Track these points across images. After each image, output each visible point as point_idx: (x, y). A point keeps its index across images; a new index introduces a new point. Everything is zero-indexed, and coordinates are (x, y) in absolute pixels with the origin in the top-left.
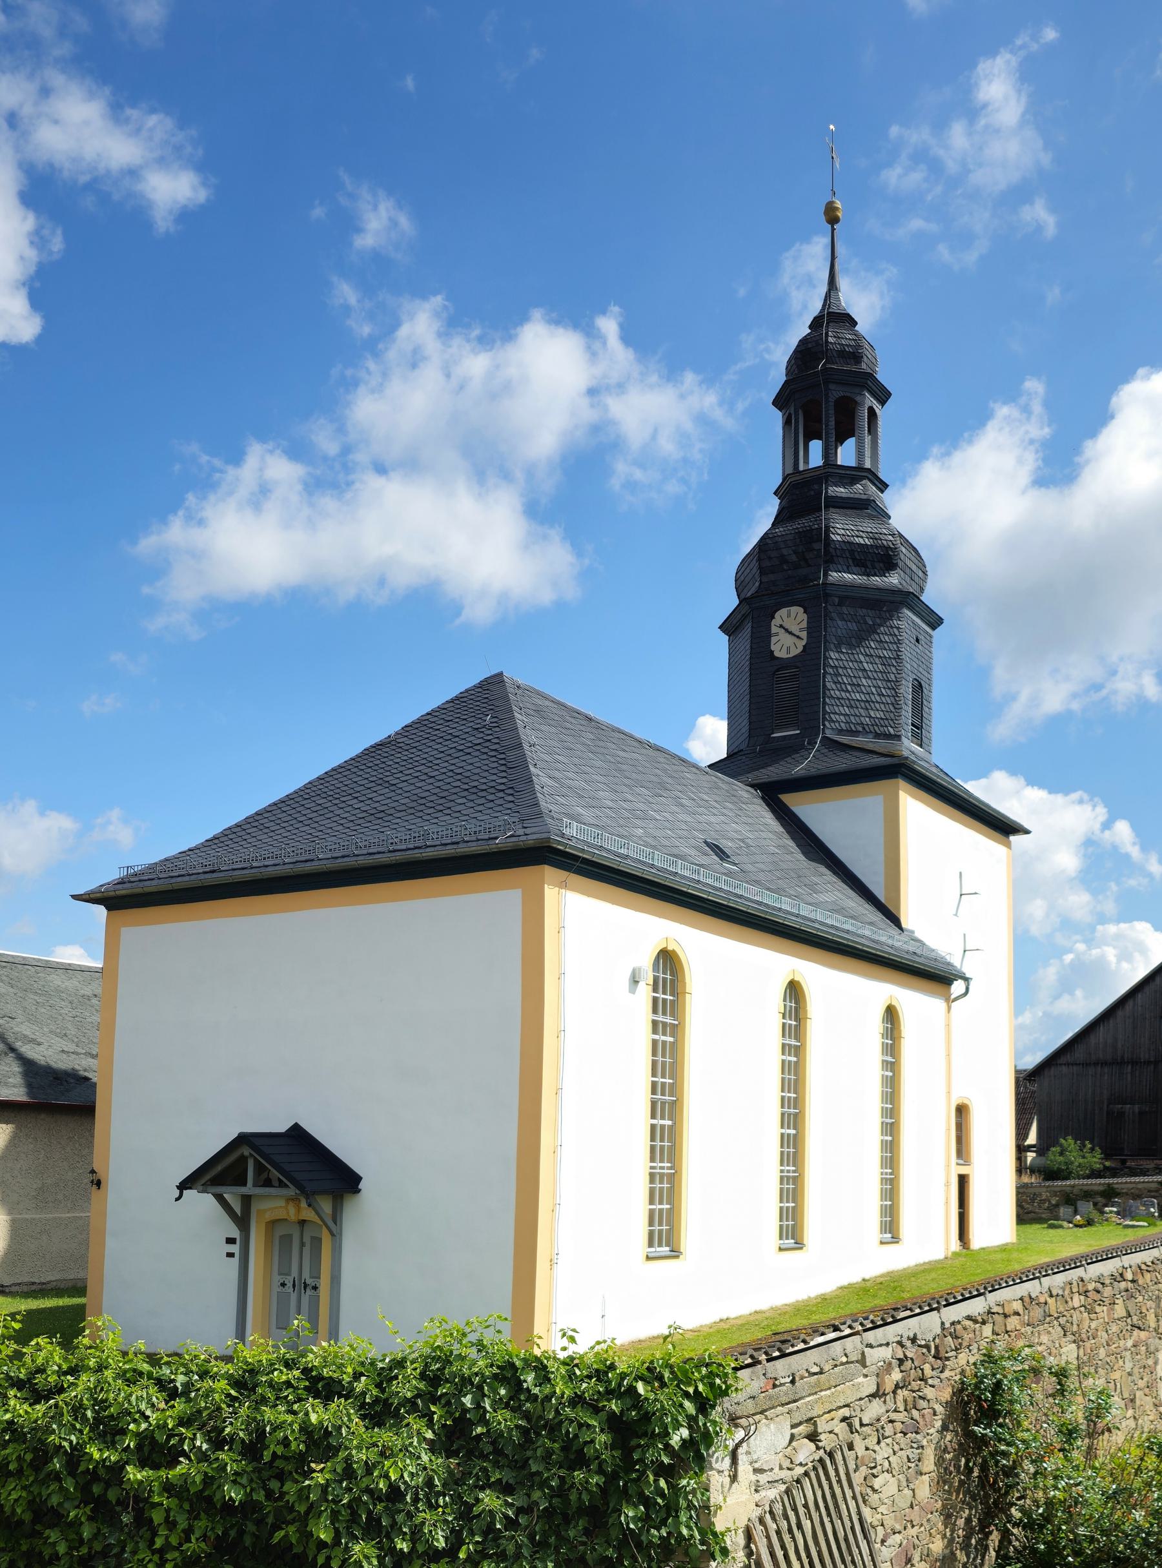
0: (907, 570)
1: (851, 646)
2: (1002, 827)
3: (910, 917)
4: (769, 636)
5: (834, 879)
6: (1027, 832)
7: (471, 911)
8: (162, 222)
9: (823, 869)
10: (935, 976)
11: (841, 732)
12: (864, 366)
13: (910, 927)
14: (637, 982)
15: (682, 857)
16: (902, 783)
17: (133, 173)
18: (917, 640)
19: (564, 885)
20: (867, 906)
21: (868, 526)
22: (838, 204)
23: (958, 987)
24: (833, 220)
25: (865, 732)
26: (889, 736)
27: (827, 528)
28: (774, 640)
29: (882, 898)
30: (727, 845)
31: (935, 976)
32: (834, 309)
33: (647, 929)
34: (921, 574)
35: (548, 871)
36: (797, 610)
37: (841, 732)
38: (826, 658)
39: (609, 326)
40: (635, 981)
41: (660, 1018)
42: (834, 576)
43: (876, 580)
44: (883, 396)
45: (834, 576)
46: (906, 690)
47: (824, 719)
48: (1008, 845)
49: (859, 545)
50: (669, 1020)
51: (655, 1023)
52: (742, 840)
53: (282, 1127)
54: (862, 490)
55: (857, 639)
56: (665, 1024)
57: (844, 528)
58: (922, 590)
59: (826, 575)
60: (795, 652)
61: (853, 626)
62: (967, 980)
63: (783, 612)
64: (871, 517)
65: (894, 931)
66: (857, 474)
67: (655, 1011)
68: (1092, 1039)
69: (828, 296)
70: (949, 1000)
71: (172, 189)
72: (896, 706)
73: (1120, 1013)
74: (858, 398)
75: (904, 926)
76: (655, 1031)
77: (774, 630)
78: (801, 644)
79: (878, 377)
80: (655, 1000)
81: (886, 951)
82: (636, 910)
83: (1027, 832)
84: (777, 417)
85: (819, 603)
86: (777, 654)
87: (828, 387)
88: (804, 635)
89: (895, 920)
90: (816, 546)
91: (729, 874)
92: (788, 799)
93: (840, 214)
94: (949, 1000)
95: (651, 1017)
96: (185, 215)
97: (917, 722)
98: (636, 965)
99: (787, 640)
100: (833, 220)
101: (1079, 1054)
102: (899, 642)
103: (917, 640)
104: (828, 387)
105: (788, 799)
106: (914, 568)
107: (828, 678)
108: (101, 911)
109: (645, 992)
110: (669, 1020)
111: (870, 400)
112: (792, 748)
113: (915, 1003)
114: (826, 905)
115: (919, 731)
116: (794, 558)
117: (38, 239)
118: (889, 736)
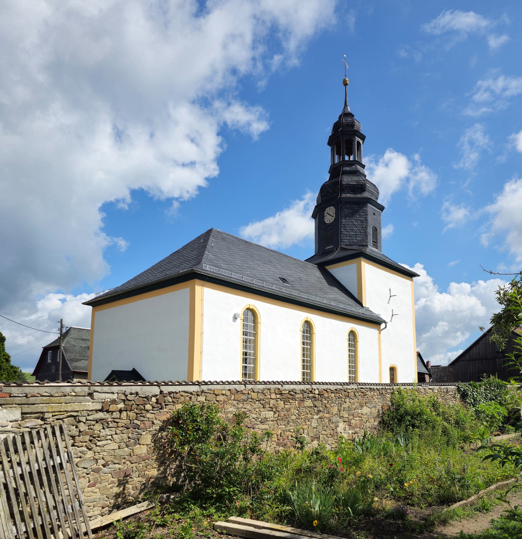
0: (370, 191)
1: (350, 217)
2: (410, 275)
3: (367, 302)
4: (324, 217)
5: (339, 291)
6: (419, 276)
7: (175, 296)
8: (256, 138)
9: (336, 289)
10: (375, 322)
11: (347, 245)
12: (355, 128)
13: (367, 306)
14: (236, 318)
15: (266, 281)
16: (362, 259)
17: (249, 124)
18: (374, 214)
19: (203, 285)
20: (351, 300)
21: (355, 178)
22: (347, 79)
23: (383, 325)
24: (346, 84)
25: (355, 245)
26: (363, 246)
27: (341, 180)
28: (325, 218)
29: (357, 297)
30: (289, 279)
31: (375, 322)
32: (346, 112)
33: (241, 302)
34: (376, 193)
35: (197, 281)
36: (332, 208)
37: (347, 245)
38: (341, 222)
39: (417, 157)
40: (235, 318)
41: (351, 348)
42: (344, 195)
43: (358, 196)
44: (363, 138)
45: (344, 195)
46: (370, 231)
47: (341, 241)
48: (412, 281)
49: (352, 185)
50: (353, 349)
51: (349, 350)
52: (299, 278)
53: (131, 369)
54: (355, 168)
55: (352, 215)
56: (307, 343)
57: (347, 180)
58: (377, 198)
59: (341, 195)
60: (332, 221)
61: (350, 211)
62: (385, 322)
63: (328, 209)
64: (357, 176)
65: (359, 307)
66: (351, 164)
67: (349, 347)
68: (472, 352)
69: (344, 108)
70: (380, 331)
71: (259, 127)
72: (366, 236)
73: (480, 342)
74: (353, 139)
75: (364, 306)
76: (349, 352)
77: (325, 214)
78: (333, 218)
79: (361, 132)
80: (349, 344)
81: (350, 312)
82: (226, 292)
83: (419, 276)
84: (329, 148)
85: (339, 204)
86: (326, 222)
87: (345, 137)
88: (334, 215)
89: (361, 304)
90: (337, 186)
91: (288, 287)
92: (328, 268)
93: (348, 82)
94: (380, 331)
95: (348, 348)
96: (262, 135)
97: (375, 241)
98: (235, 312)
99: (330, 217)
100: (346, 84)
101: (467, 357)
102: (367, 215)
103: (374, 214)
104: (345, 137)
105: (328, 268)
106: (373, 191)
107: (342, 228)
108: (90, 307)
109: (239, 322)
110: (353, 349)
111: (357, 139)
112: (331, 252)
113: (364, 332)
114: (334, 298)
115: (376, 243)
116: (331, 191)
117: (221, 145)
118: (363, 246)
